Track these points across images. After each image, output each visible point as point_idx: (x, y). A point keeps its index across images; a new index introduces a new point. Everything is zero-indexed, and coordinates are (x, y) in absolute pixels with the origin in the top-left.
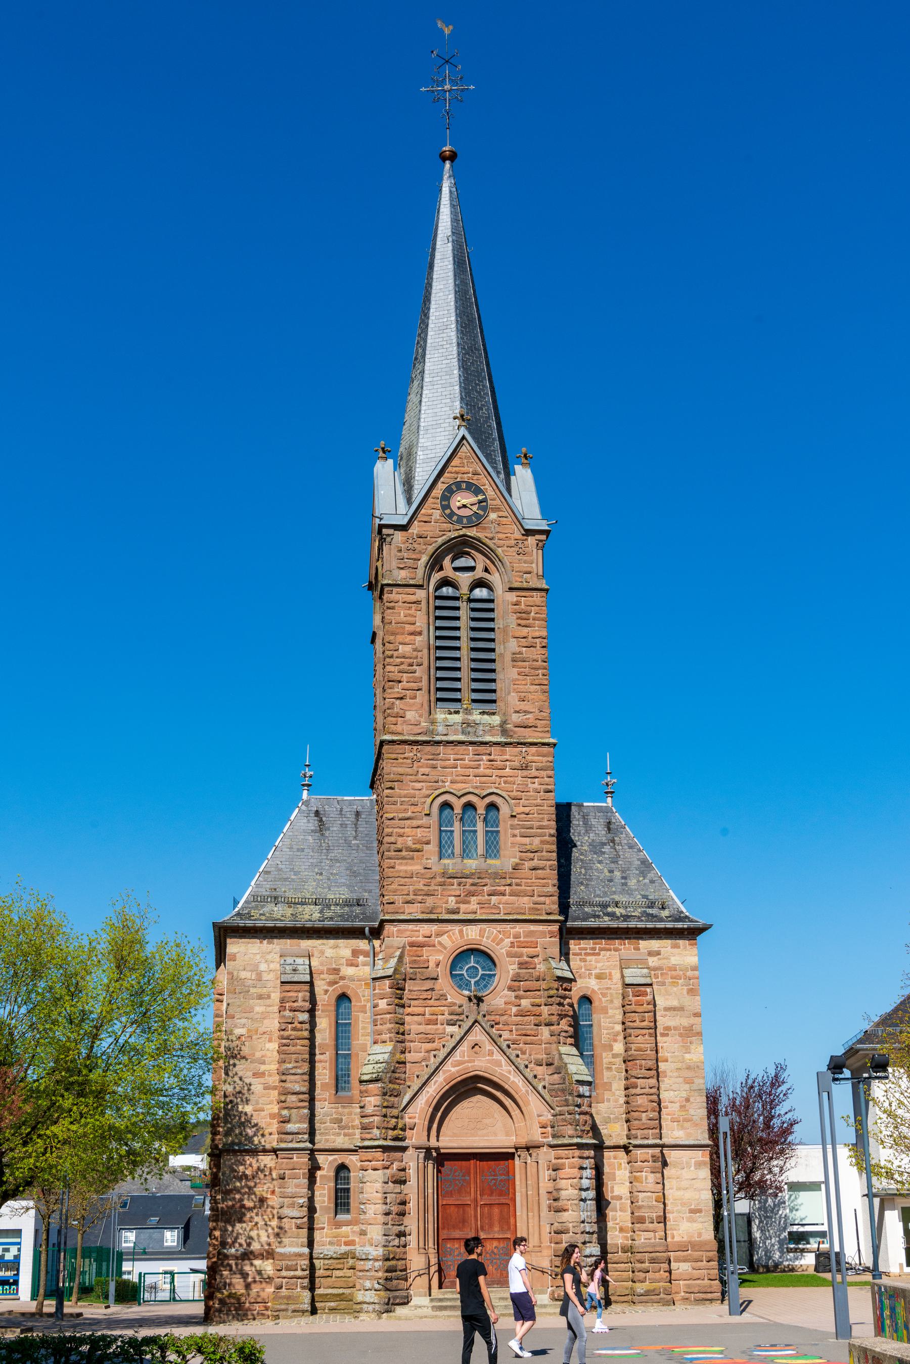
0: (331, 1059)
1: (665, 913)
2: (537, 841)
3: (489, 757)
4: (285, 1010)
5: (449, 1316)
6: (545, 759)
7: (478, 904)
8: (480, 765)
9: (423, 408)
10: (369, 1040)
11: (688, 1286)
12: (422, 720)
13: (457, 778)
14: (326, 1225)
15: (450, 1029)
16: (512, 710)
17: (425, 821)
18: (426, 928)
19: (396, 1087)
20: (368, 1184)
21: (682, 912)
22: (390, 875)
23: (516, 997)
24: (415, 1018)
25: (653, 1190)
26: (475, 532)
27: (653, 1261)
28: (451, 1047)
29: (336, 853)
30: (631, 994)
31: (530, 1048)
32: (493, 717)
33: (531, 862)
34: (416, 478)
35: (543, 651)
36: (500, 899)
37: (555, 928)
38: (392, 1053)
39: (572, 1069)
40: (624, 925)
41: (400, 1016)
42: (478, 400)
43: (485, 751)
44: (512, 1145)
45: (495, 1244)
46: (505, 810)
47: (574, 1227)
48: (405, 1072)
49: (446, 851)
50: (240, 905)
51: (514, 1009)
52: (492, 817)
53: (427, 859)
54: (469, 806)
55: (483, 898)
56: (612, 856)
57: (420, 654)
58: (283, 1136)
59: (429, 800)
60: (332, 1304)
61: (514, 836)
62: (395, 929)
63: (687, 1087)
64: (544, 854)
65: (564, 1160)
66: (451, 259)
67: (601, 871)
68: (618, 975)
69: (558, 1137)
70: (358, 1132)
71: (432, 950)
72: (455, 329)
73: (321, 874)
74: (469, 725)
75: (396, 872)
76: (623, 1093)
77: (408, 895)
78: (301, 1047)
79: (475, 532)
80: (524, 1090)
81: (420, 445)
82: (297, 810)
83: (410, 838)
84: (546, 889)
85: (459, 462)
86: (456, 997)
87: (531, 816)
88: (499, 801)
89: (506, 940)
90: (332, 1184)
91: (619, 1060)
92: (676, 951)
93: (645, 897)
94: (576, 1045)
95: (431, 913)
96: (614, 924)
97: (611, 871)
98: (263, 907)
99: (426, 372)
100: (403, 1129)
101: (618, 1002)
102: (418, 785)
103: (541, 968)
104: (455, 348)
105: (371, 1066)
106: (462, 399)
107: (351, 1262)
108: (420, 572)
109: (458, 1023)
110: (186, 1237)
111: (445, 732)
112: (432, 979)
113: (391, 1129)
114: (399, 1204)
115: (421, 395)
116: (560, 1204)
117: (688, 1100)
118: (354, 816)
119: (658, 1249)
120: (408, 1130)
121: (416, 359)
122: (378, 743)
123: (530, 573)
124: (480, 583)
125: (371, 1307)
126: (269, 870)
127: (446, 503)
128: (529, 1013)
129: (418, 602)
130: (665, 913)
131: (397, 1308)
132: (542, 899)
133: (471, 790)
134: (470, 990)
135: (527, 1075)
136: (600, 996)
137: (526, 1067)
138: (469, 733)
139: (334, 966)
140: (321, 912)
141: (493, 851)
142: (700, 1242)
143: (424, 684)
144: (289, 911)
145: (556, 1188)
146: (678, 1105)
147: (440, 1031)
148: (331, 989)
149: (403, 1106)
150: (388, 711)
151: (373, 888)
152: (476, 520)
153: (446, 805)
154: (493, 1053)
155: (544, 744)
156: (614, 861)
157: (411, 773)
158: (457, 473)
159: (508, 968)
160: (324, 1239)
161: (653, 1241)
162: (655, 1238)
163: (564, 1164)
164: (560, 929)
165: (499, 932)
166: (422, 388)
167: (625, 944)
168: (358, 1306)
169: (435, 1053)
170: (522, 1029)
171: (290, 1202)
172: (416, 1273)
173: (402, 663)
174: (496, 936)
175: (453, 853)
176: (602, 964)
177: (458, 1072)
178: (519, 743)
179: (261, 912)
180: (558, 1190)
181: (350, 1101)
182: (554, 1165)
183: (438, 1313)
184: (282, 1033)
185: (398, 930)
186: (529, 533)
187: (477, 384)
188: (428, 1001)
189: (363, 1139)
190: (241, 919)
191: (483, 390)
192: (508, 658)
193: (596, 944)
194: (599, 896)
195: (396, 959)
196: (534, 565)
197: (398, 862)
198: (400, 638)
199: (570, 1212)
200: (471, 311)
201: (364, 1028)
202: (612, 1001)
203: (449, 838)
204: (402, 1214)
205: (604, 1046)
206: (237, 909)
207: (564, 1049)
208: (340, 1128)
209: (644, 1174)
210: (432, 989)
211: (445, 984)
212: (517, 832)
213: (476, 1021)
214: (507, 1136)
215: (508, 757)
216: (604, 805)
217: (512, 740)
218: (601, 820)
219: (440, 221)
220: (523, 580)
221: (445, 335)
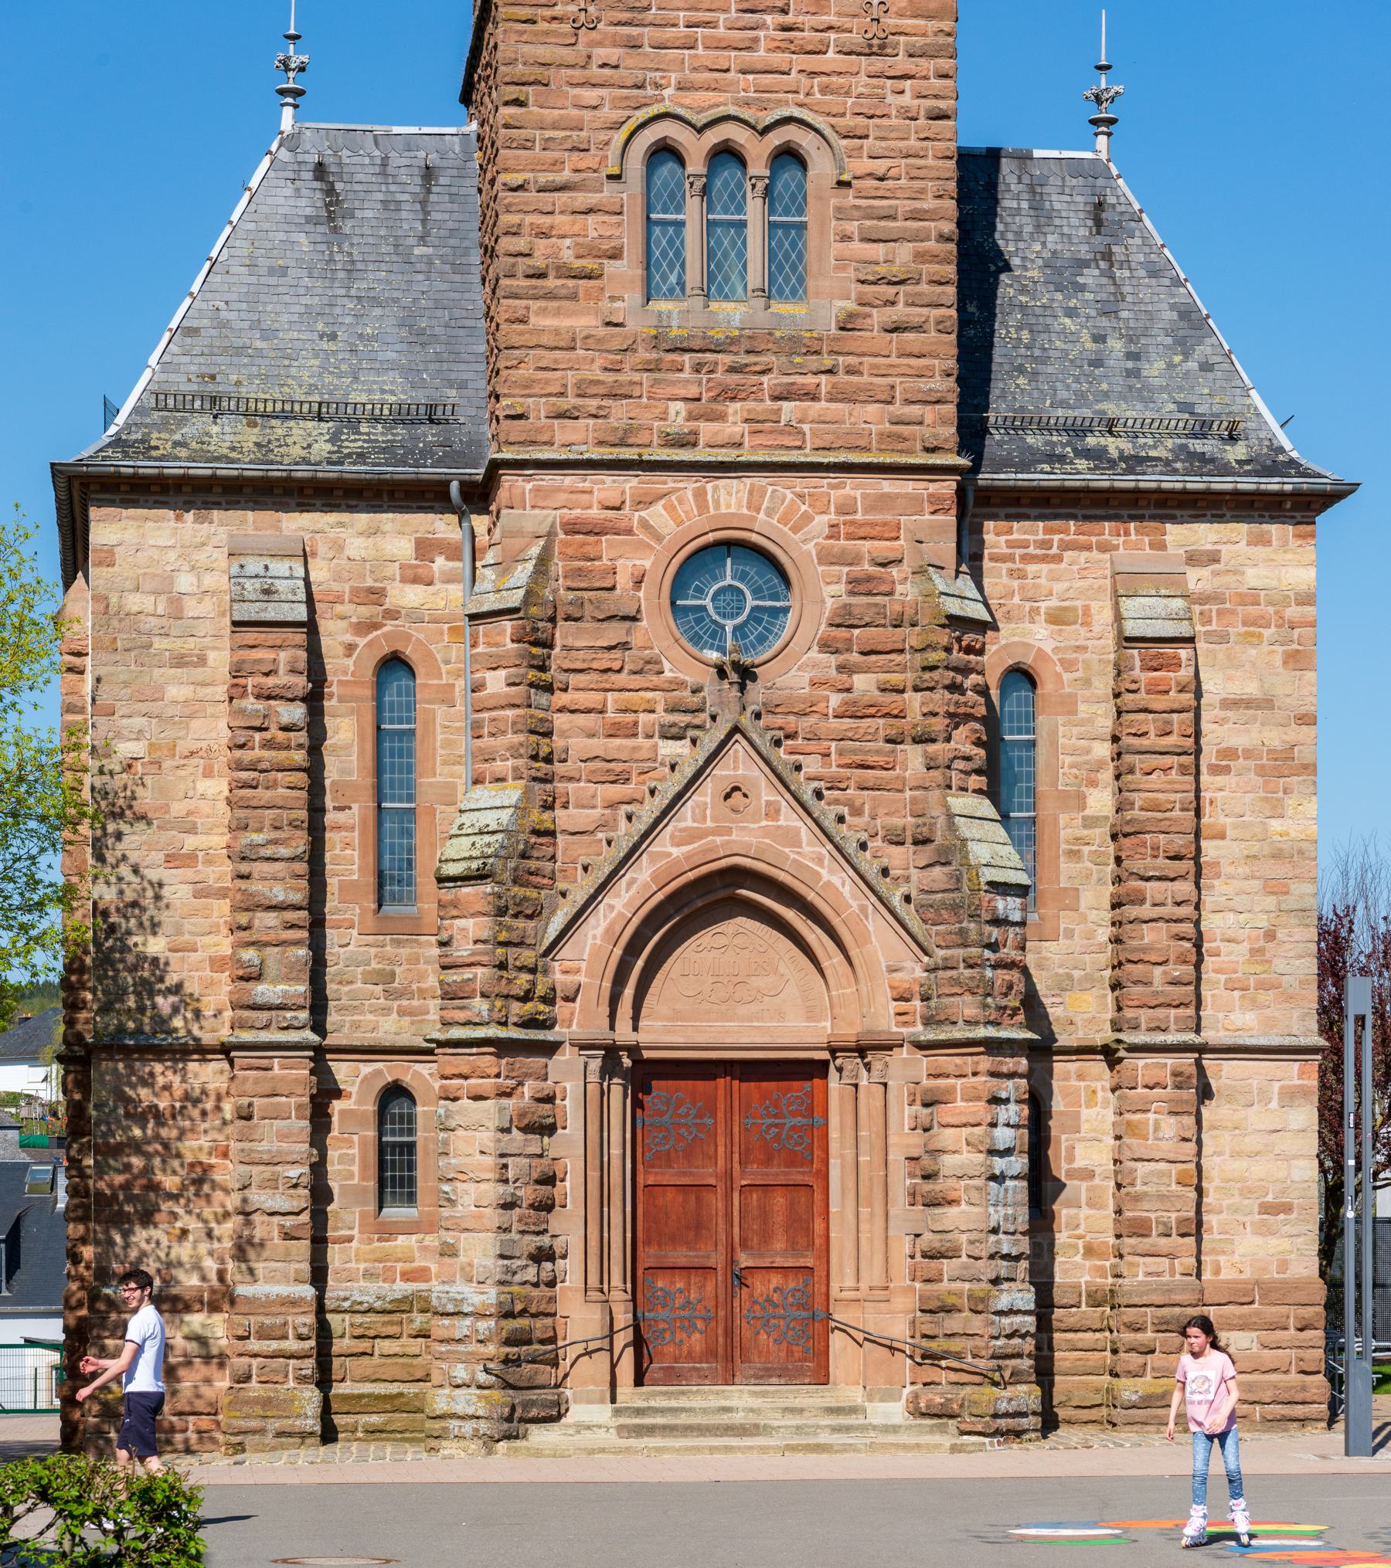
0: (363, 821)
1: (1236, 452)
2: (904, 252)
3: (781, 19)
4: (244, 695)
5: (658, 1450)
6: (933, 25)
7: (746, 421)
8: (756, 40)
10: (461, 774)
14: (355, 1232)
15: (669, 749)
17: (609, 193)
19: (532, 893)
20: (460, 1132)
21: (1281, 450)
22: (516, 340)
23: (841, 668)
24: (581, 719)
25: (1171, 1157)
28: (670, 795)
29: (371, 281)
30: (1138, 664)
31: (873, 799)
33: (888, 310)
36: (805, 411)
38: (521, 810)
39: (979, 852)
40: (1126, 482)
41: (541, 714)
44: (823, 1040)
45: (776, 1280)
46: (821, 167)
47: (972, 1242)
48: (553, 858)
49: (665, 278)
50: (121, 419)
51: (835, 700)
52: (787, 186)
53: (612, 298)
54: (727, 154)
56: (1104, 296)
58: (246, 1014)
59: (620, 137)
60: (374, 1419)
61: (846, 238)
62: (529, 486)
63: (1270, 902)
64: (924, 287)
65: (951, 1081)
67: (1071, 338)
68: (1108, 615)
69: (940, 1022)
70: (434, 1005)
71: (625, 543)
73: (333, 337)
75: (531, 332)
76: (1108, 916)
80: (854, 904)
82: (266, 161)
83: (568, 242)
84: (924, 384)
87: (890, 183)
89: (818, 519)
90: (371, 1133)
92: (1261, 551)
93: (1185, 407)
95: (622, 444)
96: (1101, 480)
97: (1099, 339)
98: (181, 423)
102: (590, 95)
103: (907, 592)
105: (466, 842)
107: (419, 1320)
109: (691, 733)
112: (625, 618)
114: (539, 1182)
116: (938, 1188)
117: (1270, 936)
119: (1177, 1298)
120: (559, 1003)
125: (468, 1427)
126: (195, 324)
128: (872, 711)
130: (1236, 452)
131: (533, 1428)
132: (915, 410)
133: (733, 110)
134: (722, 649)
135: (863, 867)
136: (1059, 668)
139: (369, 583)
140: (334, 439)
141: (787, 280)
142: (1284, 1281)
144: (250, 437)
145: (931, 1147)
146: (1246, 945)
148: (362, 642)
149: (547, 943)
153: (665, 152)
154: (778, 811)
160: (353, 1265)
161: (1166, 1278)
162: (1172, 1273)
163: (951, 1090)
165: (801, 496)
167: (1127, 533)
168: (437, 1425)
169: (629, 808)
170: (854, 752)
171: (267, 1175)
172: (579, 1349)
175: (681, 284)
176: (1067, 585)
177: (688, 857)
179: (177, 437)
180: (935, 1153)
181: (413, 930)
182: (927, 1091)
183: (632, 1442)
184: (238, 753)
185: (537, 490)
188: (614, 677)
189: (446, 1024)
194: (1064, 404)
195: (530, 566)
197: (535, 305)
199: (964, 1206)
201: (447, 744)
202: (1087, 682)
205: (1064, 796)
206: (113, 430)
207: (960, 803)
209: (1151, 1116)
210: (625, 646)
212: (852, 227)
213: (736, 729)
214: (810, 1019)
215: (831, 19)
216: (1089, 155)
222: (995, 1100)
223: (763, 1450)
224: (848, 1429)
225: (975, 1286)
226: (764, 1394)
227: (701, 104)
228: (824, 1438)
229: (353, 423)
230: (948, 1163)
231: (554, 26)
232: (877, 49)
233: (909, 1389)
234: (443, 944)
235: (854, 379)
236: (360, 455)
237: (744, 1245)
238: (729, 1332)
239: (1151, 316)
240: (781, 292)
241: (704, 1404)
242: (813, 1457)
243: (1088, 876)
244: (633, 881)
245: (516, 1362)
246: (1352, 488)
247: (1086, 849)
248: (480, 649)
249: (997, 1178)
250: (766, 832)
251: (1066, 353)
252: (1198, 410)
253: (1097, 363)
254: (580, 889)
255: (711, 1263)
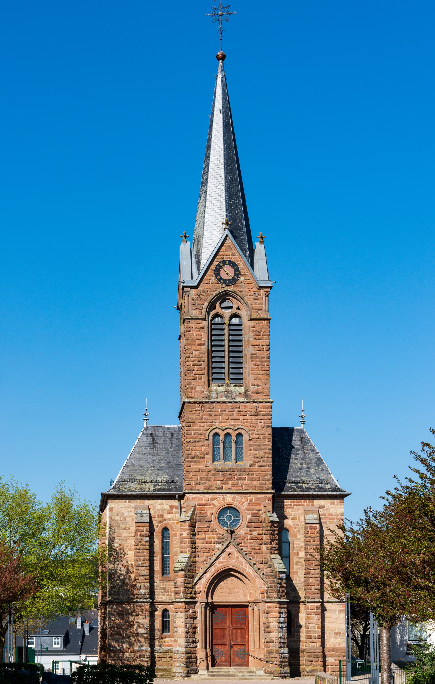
0: (160, 559)
1: (328, 486)
2: (262, 452)
4: (137, 536)
5: (215, 679)
6: (267, 410)
8: (233, 414)
9: (206, 215)
10: (178, 550)
11: (332, 668)
12: (205, 390)
13: (222, 420)
15: (217, 546)
16: (251, 384)
17: (206, 442)
18: (206, 497)
19: (192, 574)
20: (178, 619)
21: (337, 486)
22: (189, 470)
24: (201, 540)
26: (232, 288)
27: (315, 656)
28: (218, 555)
29: (161, 456)
32: (241, 388)
33: (259, 463)
34: (202, 256)
35: (267, 352)
36: (243, 482)
37: (270, 496)
38: (189, 558)
39: (276, 566)
40: (306, 493)
41: (193, 540)
42: (235, 209)
43: (236, 406)
44: (248, 601)
45: (239, 647)
46: (246, 437)
48: (196, 567)
49: (217, 458)
50: (114, 483)
51: (249, 536)
52: (240, 440)
53: (207, 462)
54: (228, 435)
55: (235, 482)
56: (302, 456)
57: (203, 356)
59: (208, 432)
60: (162, 673)
61: (251, 450)
64: (266, 459)
65: (271, 609)
66: (222, 124)
67: (296, 465)
68: (303, 518)
69: (269, 598)
70: (173, 594)
72: (223, 168)
73: (154, 467)
74: (228, 392)
75: (191, 468)
76: (303, 576)
77: (197, 480)
78: (146, 554)
79: (232, 288)
80: (253, 575)
81: (204, 237)
82: (141, 433)
83: (198, 452)
84: (266, 477)
85: (225, 249)
86: (221, 530)
88: (243, 432)
89: (246, 502)
90: (161, 618)
91: (302, 560)
92: (333, 506)
93: (318, 478)
94: (280, 554)
95: (209, 489)
96: (301, 493)
97: (301, 464)
98: (126, 484)
99: (208, 193)
100: (195, 593)
101: (302, 531)
102: (202, 424)
103: (263, 516)
104: (223, 179)
105: (179, 564)
106: (227, 210)
107: (170, 654)
108: (204, 311)
109: (222, 543)
110: (67, 642)
111: (216, 397)
112: (209, 522)
113: (189, 593)
114: (193, 628)
115: (205, 207)
118: (170, 436)
119: (317, 651)
121: (202, 183)
122: (182, 403)
123: (261, 310)
124: (235, 315)
125: (180, 675)
126: (128, 465)
127: (217, 272)
129: (203, 328)
130: (328, 486)
131: (192, 675)
132: (264, 482)
133: (229, 427)
134: (228, 528)
135: (255, 568)
137: (255, 564)
138: (228, 397)
139: (161, 514)
140: (154, 487)
141: (240, 457)
142: (339, 648)
143: (206, 371)
144: (139, 486)
147: (213, 547)
148: (159, 525)
149: (194, 583)
150: (188, 386)
151: (180, 474)
152: (233, 282)
153: (216, 434)
155: (266, 402)
156: (303, 459)
157: (199, 418)
158: (224, 255)
159: (246, 516)
161: (315, 647)
162: (317, 646)
163: (272, 611)
164: (273, 497)
165: (243, 498)
166: (206, 202)
167: (307, 502)
168: (174, 674)
169: (210, 557)
170: (253, 546)
172: (201, 660)
173: (194, 361)
174: (241, 501)
175: (220, 459)
177: (221, 567)
178: (253, 402)
179: (125, 487)
180: (269, 623)
181: (170, 579)
182: (267, 611)
183: (211, 678)
184: (136, 547)
185: (193, 498)
186: (261, 288)
187: (235, 200)
188: (207, 533)
189: (176, 598)
190: (115, 491)
191: (239, 203)
192: (248, 357)
193: (291, 502)
194: (294, 477)
195: (191, 512)
196: (263, 306)
197: (192, 463)
198: (193, 347)
199: (274, 633)
200: (232, 155)
201: (176, 544)
202: (299, 531)
203: (218, 451)
204: (194, 633)
205: (295, 553)
206: (113, 486)
207: (273, 556)
208: (164, 592)
209: (312, 615)
210: (209, 527)
211: (215, 524)
212: (252, 448)
213: (230, 543)
214: (245, 597)
215: (248, 409)
216: (300, 428)
217: (250, 400)
218: (298, 437)
219: (216, 99)
220: (258, 314)
221: (218, 171)
222: (280, 613)
223: (236, 679)
224: (252, 676)
225: (276, 648)
226: (236, 669)
227: (224, 425)
228: (247, 677)
229: (158, 484)
230: (271, 625)
231: (196, 412)
232: (257, 414)
233: (264, 668)
234: (175, 583)
235: (253, 476)
236: (159, 490)
237: (232, 640)
238: (230, 657)
239: (312, 460)
240: (239, 460)
241: (225, 671)
242: (245, 681)
243: (300, 569)
244: (211, 571)
245: (190, 662)
246: (350, 494)
247: (299, 563)
248: (182, 527)
249: (282, 628)
250: (236, 562)
251: (295, 467)
252: (321, 478)
253: (301, 469)
254: (201, 573)
255: (226, 644)
